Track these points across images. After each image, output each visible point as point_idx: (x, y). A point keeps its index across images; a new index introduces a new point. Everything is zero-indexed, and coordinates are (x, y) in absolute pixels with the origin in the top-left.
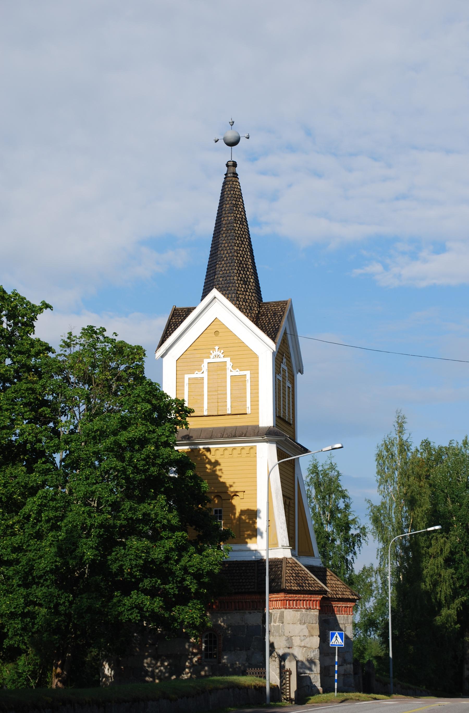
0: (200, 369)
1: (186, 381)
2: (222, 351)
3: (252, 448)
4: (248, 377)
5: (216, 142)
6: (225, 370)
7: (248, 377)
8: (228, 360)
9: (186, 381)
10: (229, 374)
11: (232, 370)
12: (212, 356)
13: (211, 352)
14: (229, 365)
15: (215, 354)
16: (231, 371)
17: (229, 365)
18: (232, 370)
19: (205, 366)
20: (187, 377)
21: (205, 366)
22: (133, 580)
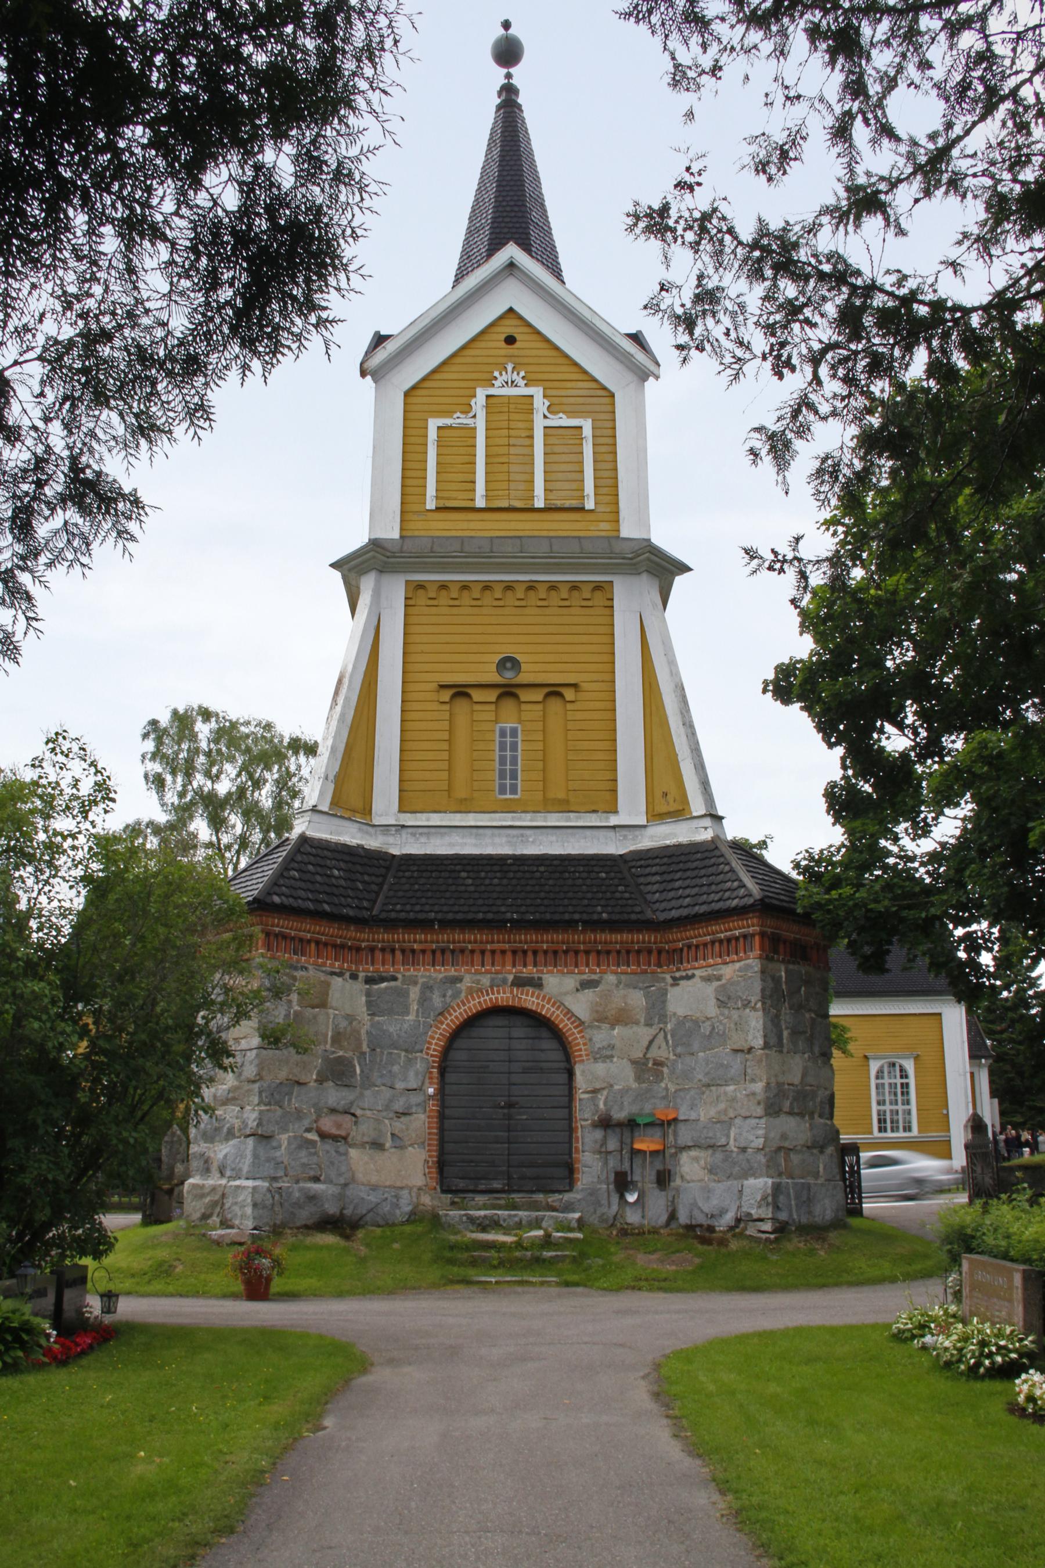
0: (467, 409)
1: (432, 434)
2: (522, 374)
3: (598, 587)
4: (587, 431)
5: (747, 78)
6: (531, 411)
7: (587, 431)
8: (537, 392)
9: (432, 434)
10: (539, 424)
11: (471, 414)
12: (497, 383)
13: (510, 367)
14: (540, 404)
15: (504, 377)
16: (545, 417)
17: (540, 404)
18: (471, 414)
19: (479, 401)
20: (433, 424)
21: (479, 401)
22: (882, 526)
